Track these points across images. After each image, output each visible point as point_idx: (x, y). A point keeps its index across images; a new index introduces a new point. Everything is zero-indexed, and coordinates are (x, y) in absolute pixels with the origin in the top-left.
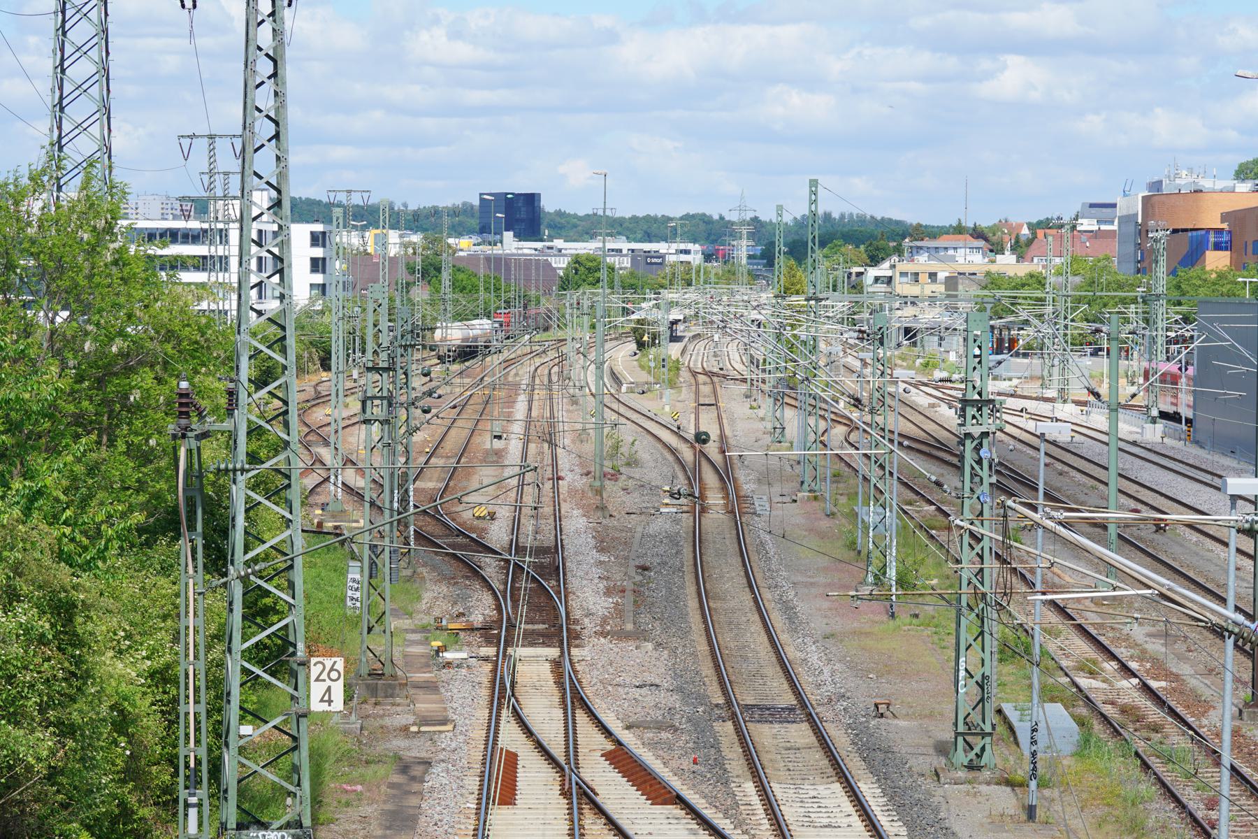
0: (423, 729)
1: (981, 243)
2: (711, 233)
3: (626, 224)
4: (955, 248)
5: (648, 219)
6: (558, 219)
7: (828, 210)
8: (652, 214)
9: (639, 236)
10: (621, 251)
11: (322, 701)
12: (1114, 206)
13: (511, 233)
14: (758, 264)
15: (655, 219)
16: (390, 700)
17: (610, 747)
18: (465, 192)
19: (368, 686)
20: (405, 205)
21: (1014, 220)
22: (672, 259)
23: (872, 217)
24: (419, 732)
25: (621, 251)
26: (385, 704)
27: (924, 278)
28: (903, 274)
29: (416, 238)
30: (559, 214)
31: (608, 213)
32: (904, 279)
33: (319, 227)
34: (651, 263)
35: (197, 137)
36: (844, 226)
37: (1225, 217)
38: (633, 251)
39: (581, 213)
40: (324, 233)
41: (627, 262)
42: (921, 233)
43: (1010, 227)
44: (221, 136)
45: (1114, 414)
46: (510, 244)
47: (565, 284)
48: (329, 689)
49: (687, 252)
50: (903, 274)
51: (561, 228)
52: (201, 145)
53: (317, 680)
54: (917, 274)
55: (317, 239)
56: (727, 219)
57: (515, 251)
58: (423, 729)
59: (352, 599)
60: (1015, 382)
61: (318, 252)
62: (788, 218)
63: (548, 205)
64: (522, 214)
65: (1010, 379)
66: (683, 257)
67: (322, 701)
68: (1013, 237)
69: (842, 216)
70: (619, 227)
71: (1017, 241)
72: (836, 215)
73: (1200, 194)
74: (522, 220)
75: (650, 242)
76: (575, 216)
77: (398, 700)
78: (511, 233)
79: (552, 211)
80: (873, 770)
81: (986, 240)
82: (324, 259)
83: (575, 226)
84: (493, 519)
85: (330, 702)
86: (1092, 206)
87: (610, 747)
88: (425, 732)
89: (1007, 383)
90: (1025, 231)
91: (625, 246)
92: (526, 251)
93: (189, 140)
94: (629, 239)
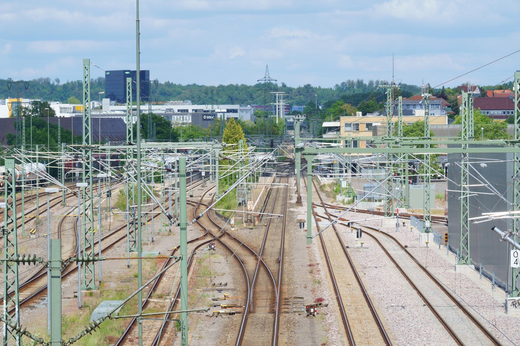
1: (442, 100)
5: (231, 87)
6: (167, 89)
8: (234, 84)
9: (225, 101)
10: (187, 111)
15: (236, 88)
20: (58, 81)
25: (187, 111)
28: (347, 125)
29: (26, 103)
30: (168, 84)
32: (348, 129)
34: (206, 120)
38: (196, 111)
39: (184, 84)
41: (188, 119)
49: (235, 111)
50: (347, 125)
51: (169, 95)
54: (358, 125)
56: (288, 86)
57: (109, 113)
62: (62, 83)
65: (380, 201)
66: (232, 115)
69: (371, 83)
70: (169, 92)
72: (366, 82)
74: (213, 107)
76: (180, 86)
79: (162, 81)
81: (445, 98)
83: (179, 93)
89: (378, 204)
91: (190, 107)
94: (194, 103)
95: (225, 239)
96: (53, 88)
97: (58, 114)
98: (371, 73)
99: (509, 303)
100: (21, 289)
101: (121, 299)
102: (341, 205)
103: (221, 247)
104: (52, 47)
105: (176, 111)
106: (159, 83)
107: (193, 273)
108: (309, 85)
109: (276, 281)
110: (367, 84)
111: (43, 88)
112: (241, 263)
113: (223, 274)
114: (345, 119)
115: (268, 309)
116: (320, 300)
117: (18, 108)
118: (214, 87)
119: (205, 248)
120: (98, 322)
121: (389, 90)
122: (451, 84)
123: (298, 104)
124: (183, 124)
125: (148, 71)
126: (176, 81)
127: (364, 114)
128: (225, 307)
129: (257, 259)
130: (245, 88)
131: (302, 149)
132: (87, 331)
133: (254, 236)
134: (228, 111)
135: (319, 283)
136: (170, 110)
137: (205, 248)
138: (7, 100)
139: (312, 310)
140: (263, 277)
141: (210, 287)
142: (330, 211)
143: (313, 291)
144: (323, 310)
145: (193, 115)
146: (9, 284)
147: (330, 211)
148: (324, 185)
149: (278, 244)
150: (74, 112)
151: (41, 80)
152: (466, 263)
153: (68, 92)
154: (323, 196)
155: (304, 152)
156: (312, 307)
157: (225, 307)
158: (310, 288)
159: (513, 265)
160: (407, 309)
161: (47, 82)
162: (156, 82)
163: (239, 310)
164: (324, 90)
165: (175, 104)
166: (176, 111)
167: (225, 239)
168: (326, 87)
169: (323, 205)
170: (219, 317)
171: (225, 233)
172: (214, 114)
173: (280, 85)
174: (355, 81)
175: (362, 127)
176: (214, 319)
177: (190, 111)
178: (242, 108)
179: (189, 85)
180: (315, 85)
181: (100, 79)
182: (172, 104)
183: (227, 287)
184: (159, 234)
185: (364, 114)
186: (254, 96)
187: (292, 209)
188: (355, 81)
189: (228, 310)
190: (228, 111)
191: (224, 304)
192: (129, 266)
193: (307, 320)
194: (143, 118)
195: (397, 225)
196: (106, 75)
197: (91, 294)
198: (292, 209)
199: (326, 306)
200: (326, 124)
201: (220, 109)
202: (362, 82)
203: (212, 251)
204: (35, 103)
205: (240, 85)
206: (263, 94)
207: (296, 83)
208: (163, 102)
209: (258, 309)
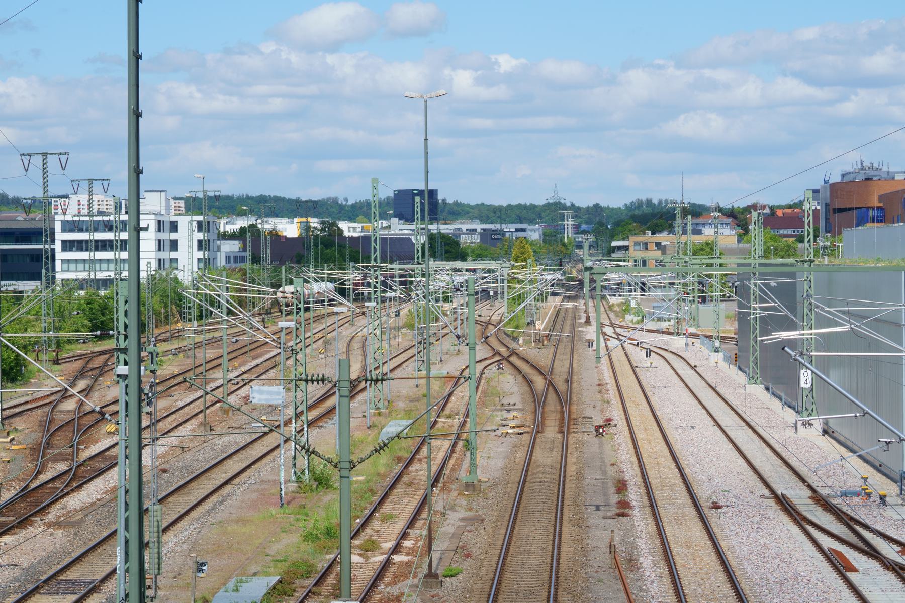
1: (730, 220)
3: (503, 211)
6: (455, 208)
7: (649, 197)
10: (475, 230)
17: (851, 576)
20: (346, 200)
25: (475, 230)
29: (314, 222)
30: (457, 204)
32: (637, 248)
34: (495, 239)
35: (34, 154)
36: (662, 208)
37: (881, 198)
38: (484, 230)
39: (472, 203)
41: (477, 239)
44: (51, 154)
45: (472, 351)
49: (524, 230)
52: (37, 161)
54: (646, 244)
56: (577, 205)
62: (350, 203)
65: (669, 320)
66: (520, 234)
69: (660, 202)
70: (458, 211)
72: (655, 201)
73: (869, 182)
75: (521, 223)
79: (451, 202)
87: (851, 576)
89: (667, 323)
91: (479, 226)
92: (406, 232)
93: (28, 157)
94: (483, 221)
95: (513, 359)
96: (341, 207)
97: (347, 234)
99: (799, 423)
100: (310, 408)
101: (409, 418)
102: (630, 325)
103: (510, 366)
104: (337, 166)
105: (464, 230)
106: (440, 197)
107: (482, 393)
108: (598, 204)
109: (565, 400)
111: (332, 207)
112: (529, 383)
113: (512, 394)
114: (634, 239)
115: (557, 429)
116: (610, 420)
117: (307, 227)
118: (7, 196)
119: (494, 368)
120: (386, 442)
121: (678, 209)
123: (587, 223)
124: (472, 243)
125: (437, 191)
126: (464, 200)
127: (653, 233)
128: (514, 427)
129: (545, 379)
130: (533, 207)
131: (591, 268)
133: (542, 357)
134: (517, 230)
135: (608, 402)
136: (459, 229)
137: (494, 368)
138: (296, 220)
139: (601, 430)
140: (552, 397)
141: (499, 407)
142: (618, 330)
143: (602, 411)
144: (612, 429)
145: (481, 234)
146: (298, 404)
147: (618, 330)
148: (613, 305)
149: (567, 364)
151: (329, 199)
153: (355, 212)
154: (612, 315)
155: (593, 271)
156: (601, 427)
157: (514, 427)
158: (598, 408)
159: (803, 385)
160: (697, 429)
161: (335, 201)
162: (444, 201)
163: (527, 429)
164: (613, 209)
165: (464, 223)
166: (464, 230)
167: (513, 359)
168: (616, 206)
169: (612, 325)
170: (508, 437)
171: (513, 353)
172: (503, 233)
173: (568, 204)
175: (652, 246)
176: (503, 439)
177: (479, 230)
178: (530, 227)
179: (478, 205)
181: (388, 198)
182: (460, 223)
183: (516, 407)
184: (447, 353)
185: (653, 233)
187: (580, 329)
189: (517, 430)
190: (517, 230)
191: (512, 424)
192: (417, 386)
193: (596, 440)
195: (687, 345)
197: (379, 414)
198: (580, 329)
199: (616, 426)
200: (615, 244)
202: (651, 201)
203: (500, 371)
204: (323, 223)
205: (528, 204)
206: (551, 213)
207: (585, 201)
208: (452, 221)
209: (546, 429)
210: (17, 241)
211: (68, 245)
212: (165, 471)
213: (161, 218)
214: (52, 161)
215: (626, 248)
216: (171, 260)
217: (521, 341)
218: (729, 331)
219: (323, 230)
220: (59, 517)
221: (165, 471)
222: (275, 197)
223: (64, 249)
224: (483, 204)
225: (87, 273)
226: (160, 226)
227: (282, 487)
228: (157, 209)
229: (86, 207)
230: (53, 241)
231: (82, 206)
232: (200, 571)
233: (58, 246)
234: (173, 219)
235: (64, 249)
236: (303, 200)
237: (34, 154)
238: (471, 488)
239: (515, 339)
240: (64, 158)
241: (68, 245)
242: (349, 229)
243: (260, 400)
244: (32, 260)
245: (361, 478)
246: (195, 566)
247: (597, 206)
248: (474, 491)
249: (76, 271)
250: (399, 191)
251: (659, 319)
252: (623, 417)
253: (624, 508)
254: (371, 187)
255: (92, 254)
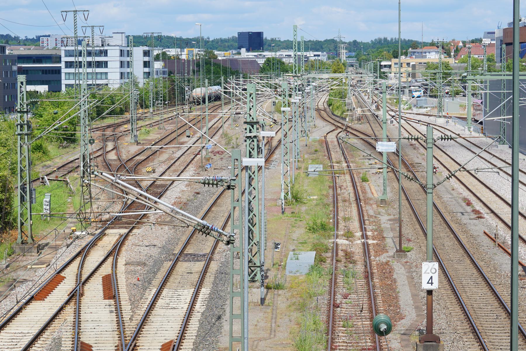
0: (33, 267)
2: (331, 46)
4: (429, 52)
7: (386, 37)
11: (428, 283)
12: (494, 33)
13: (245, 49)
14: (353, 60)
16: (30, 254)
18: (230, 32)
19: (20, 248)
21: (457, 40)
22: (313, 59)
23: (404, 40)
24: (31, 268)
26: (28, 256)
27: (404, 65)
28: (396, 64)
31: (402, 37)
32: (396, 66)
33: (146, 48)
35: (69, 11)
40: (149, 51)
41: (292, 60)
42: (415, 45)
43: (454, 43)
44: (79, 11)
46: (245, 54)
47: (263, 70)
48: (431, 278)
50: (396, 64)
51: (329, 159)
52: (71, 15)
53: (425, 273)
55: (146, 53)
57: (246, 57)
58: (33, 267)
59: (46, 209)
60: (429, 109)
61: (147, 59)
62: (211, 40)
63: (267, 36)
64: (254, 41)
65: (427, 108)
67: (428, 283)
68: (456, 46)
69: (392, 39)
70: (288, 45)
71: (457, 49)
72: (389, 39)
77: (33, 254)
78: (245, 49)
79: (269, 38)
80: (215, 284)
82: (149, 62)
84: (154, 172)
85: (432, 283)
86: (489, 33)
88: (34, 268)
89: (426, 109)
90: (461, 44)
92: (251, 57)
98: (390, 33)
104: (190, 18)
108: (355, 41)
110: (390, 40)
122: (447, 40)
124: (289, 63)
132: (447, 178)
134: (315, 56)
136: (281, 55)
150: (224, 56)
152: (504, 144)
153: (223, 44)
162: (266, 39)
168: (366, 42)
174: (383, 38)
180: (359, 40)
186: (323, 46)
188: (383, 38)
190: (315, 56)
194: (268, 60)
196: (238, 35)
200: (383, 63)
201: (311, 54)
202: (386, 39)
207: (348, 39)
210: (34, 62)
211: (69, 65)
212: (198, 193)
213: (123, 48)
214: (80, 15)
215: (390, 66)
216: (87, 73)
217: (347, 120)
218: (464, 114)
219: (205, 55)
220: (157, 219)
221: (198, 193)
222: (167, 36)
223: (66, 67)
224: (288, 40)
225: (74, 81)
226: (122, 53)
227: (283, 202)
228: (120, 43)
229: (60, 42)
230: (60, 61)
231: (58, 42)
232: (276, 248)
233: (63, 65)
234: (128, 49)
235: (66, 67)
236: (282, 40)
237: (69, 11)
238: (384, 203)
239: (344, 119)
240: (86, 13)
241: (69, 65)
242: (221, 55)
243: (382, 150)
244: (43, 73)
245: (315, 197)
246: (273, 245)
247: (355, 42)
248: (386, 204)
249: (101, 79)
250: (241, 33)
251: (421, 107)
252: (439, 163)
253: (480, 217)
254: (293, 31)
255: (94, 69)
